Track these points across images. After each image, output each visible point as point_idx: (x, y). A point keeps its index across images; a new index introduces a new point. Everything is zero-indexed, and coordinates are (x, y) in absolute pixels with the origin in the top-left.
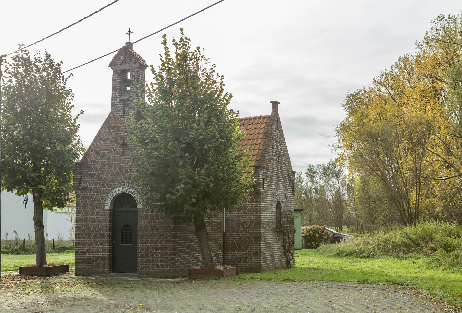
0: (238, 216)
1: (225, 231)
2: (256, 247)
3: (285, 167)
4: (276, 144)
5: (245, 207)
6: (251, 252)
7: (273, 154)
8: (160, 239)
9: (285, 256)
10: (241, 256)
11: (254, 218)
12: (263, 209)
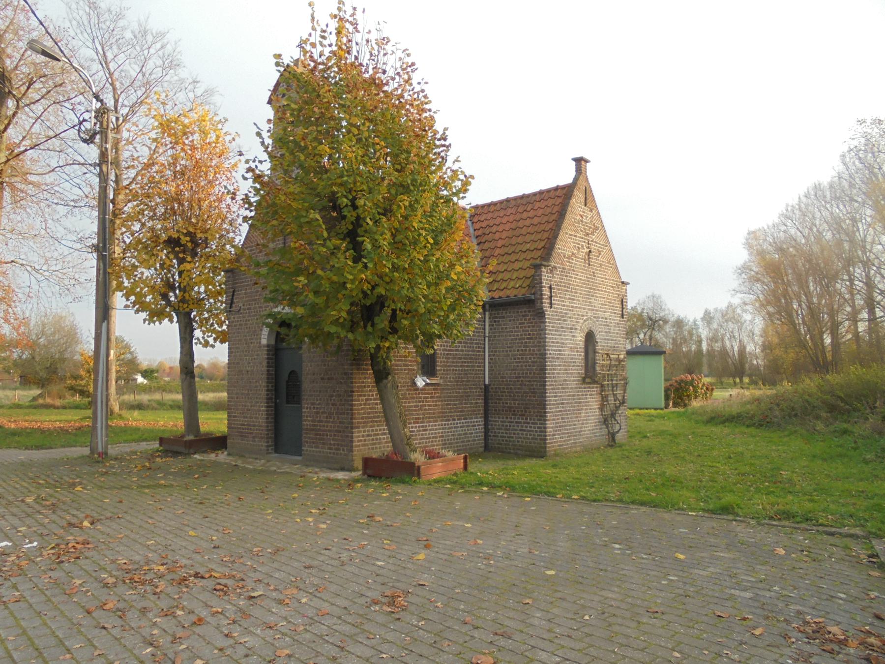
0: (508, 355)
1: (487, 382)
2: (538, 412)
3: (604, 272)
4: (581, 231)
5: (520, 339)
6: (531, 420)
7: (575, 246)
8: (332, 396)
9: (604, 426)
10: (514, 426)
11: (534, 358)
12: (553, 342)
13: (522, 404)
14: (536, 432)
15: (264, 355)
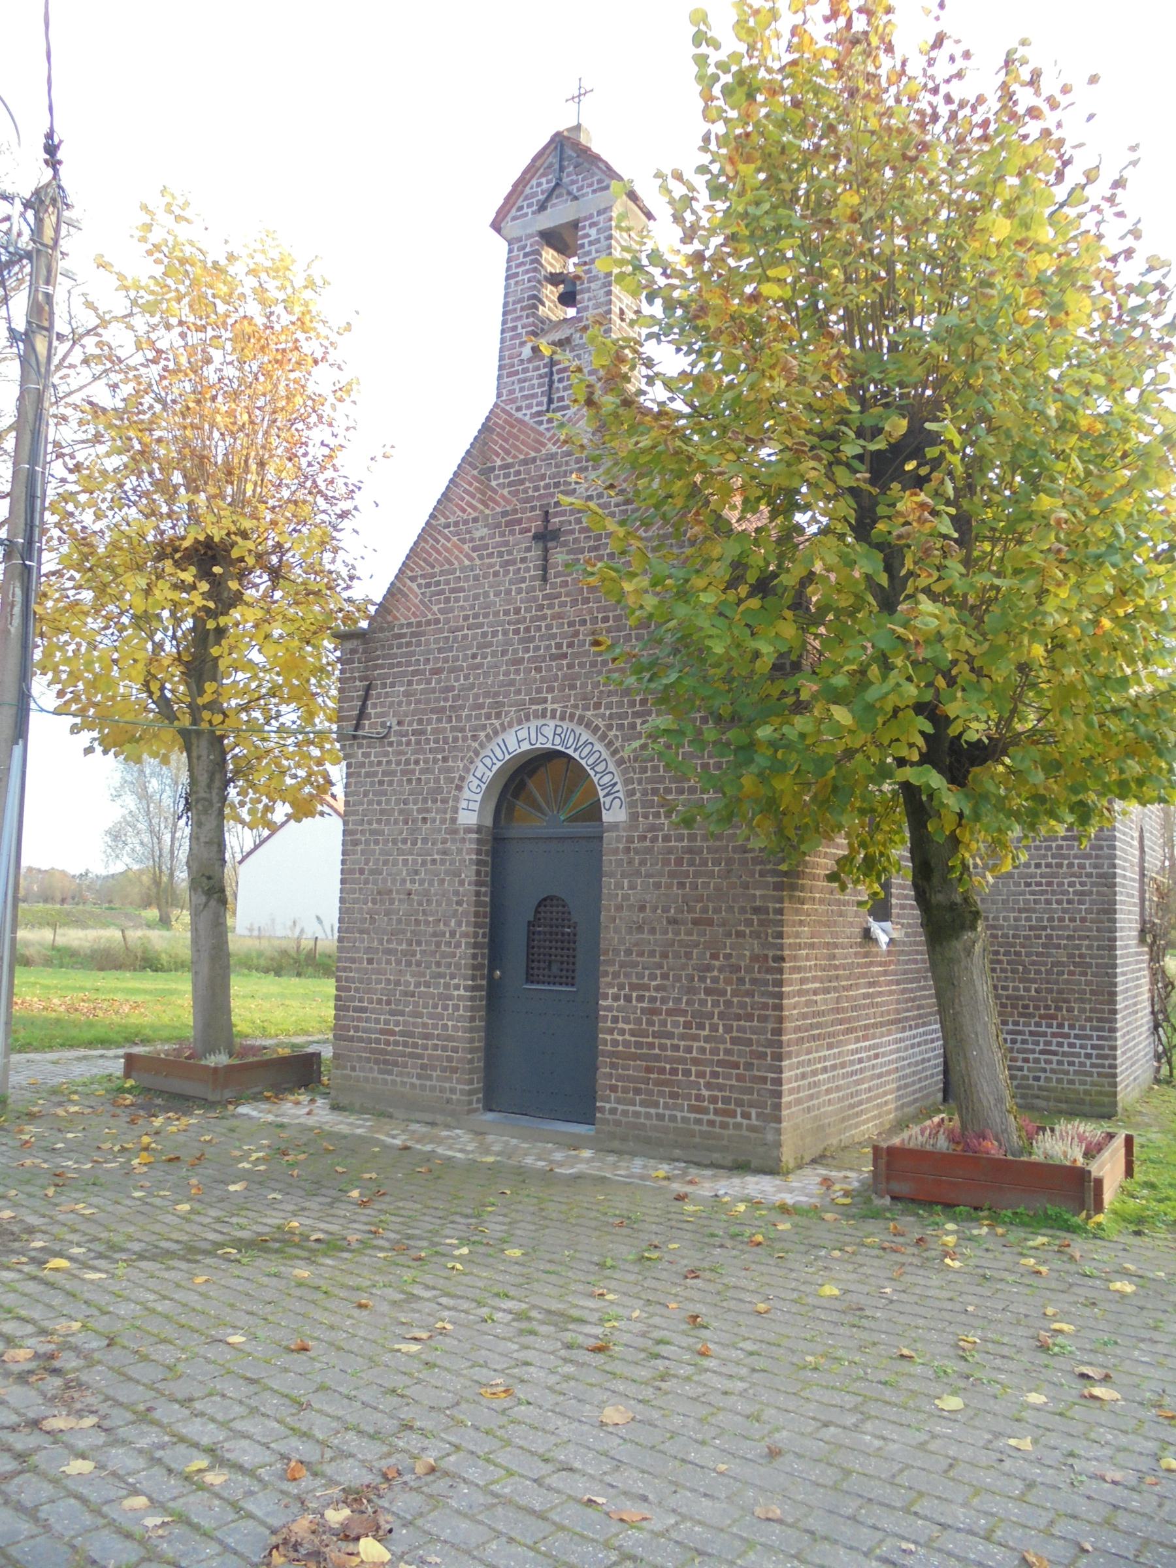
6: (1072, 1027)
8: (709, 968)
10: (1024, 1042)
11: (1082, 884)
13: (1050, 991)
14: (1088, 1056)
15: (467, 853)
